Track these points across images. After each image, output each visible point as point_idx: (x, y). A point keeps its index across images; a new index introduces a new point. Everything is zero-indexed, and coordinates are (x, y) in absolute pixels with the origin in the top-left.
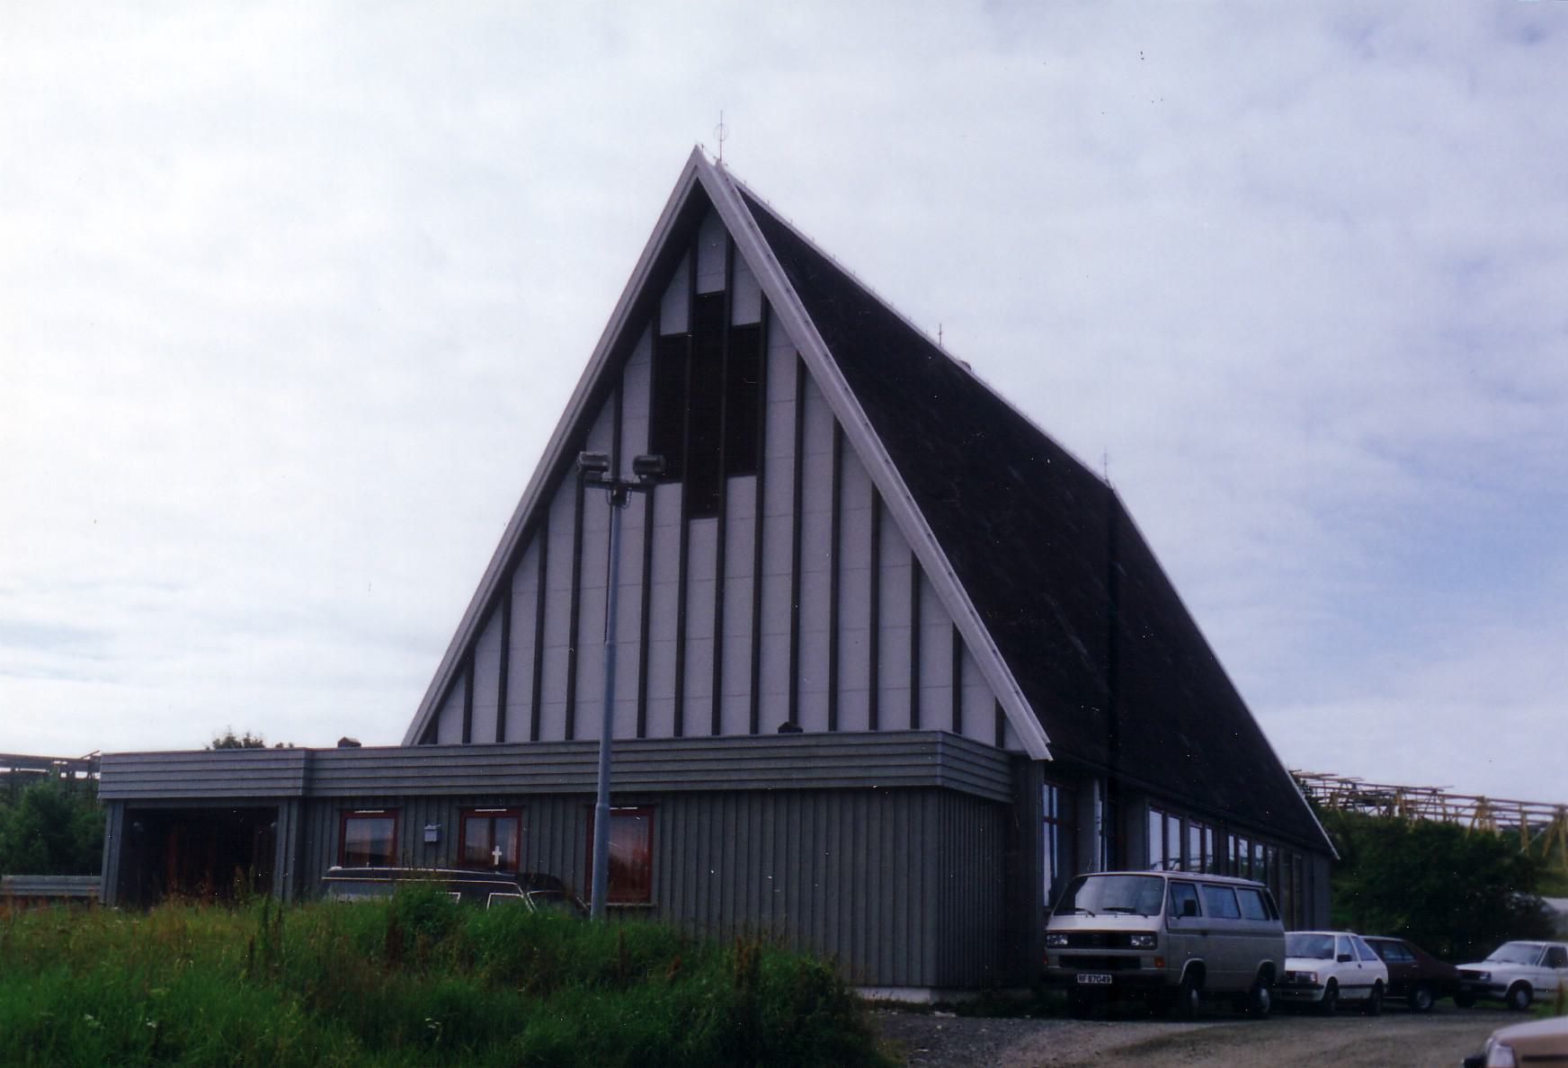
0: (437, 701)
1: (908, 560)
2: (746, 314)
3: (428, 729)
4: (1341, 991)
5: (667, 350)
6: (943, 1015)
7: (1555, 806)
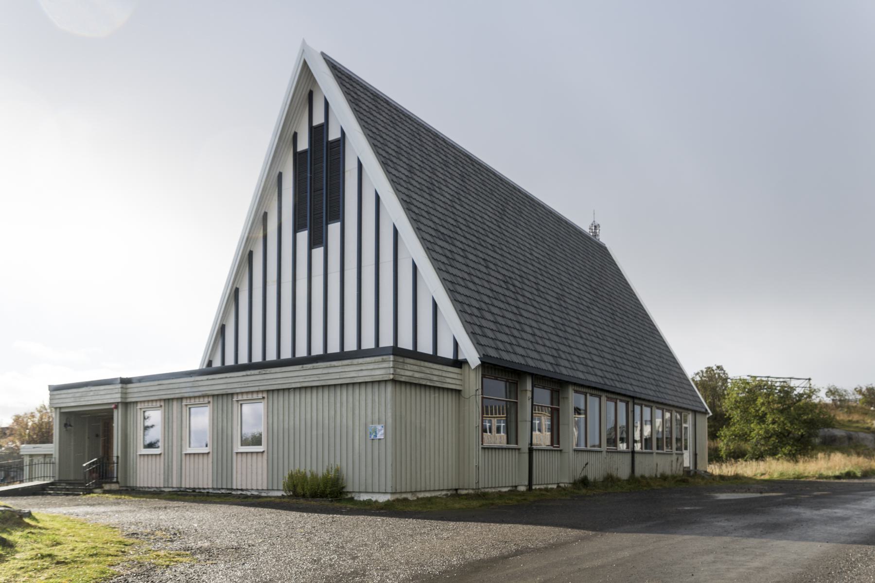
2: (334, 135)
5: (299, 157)
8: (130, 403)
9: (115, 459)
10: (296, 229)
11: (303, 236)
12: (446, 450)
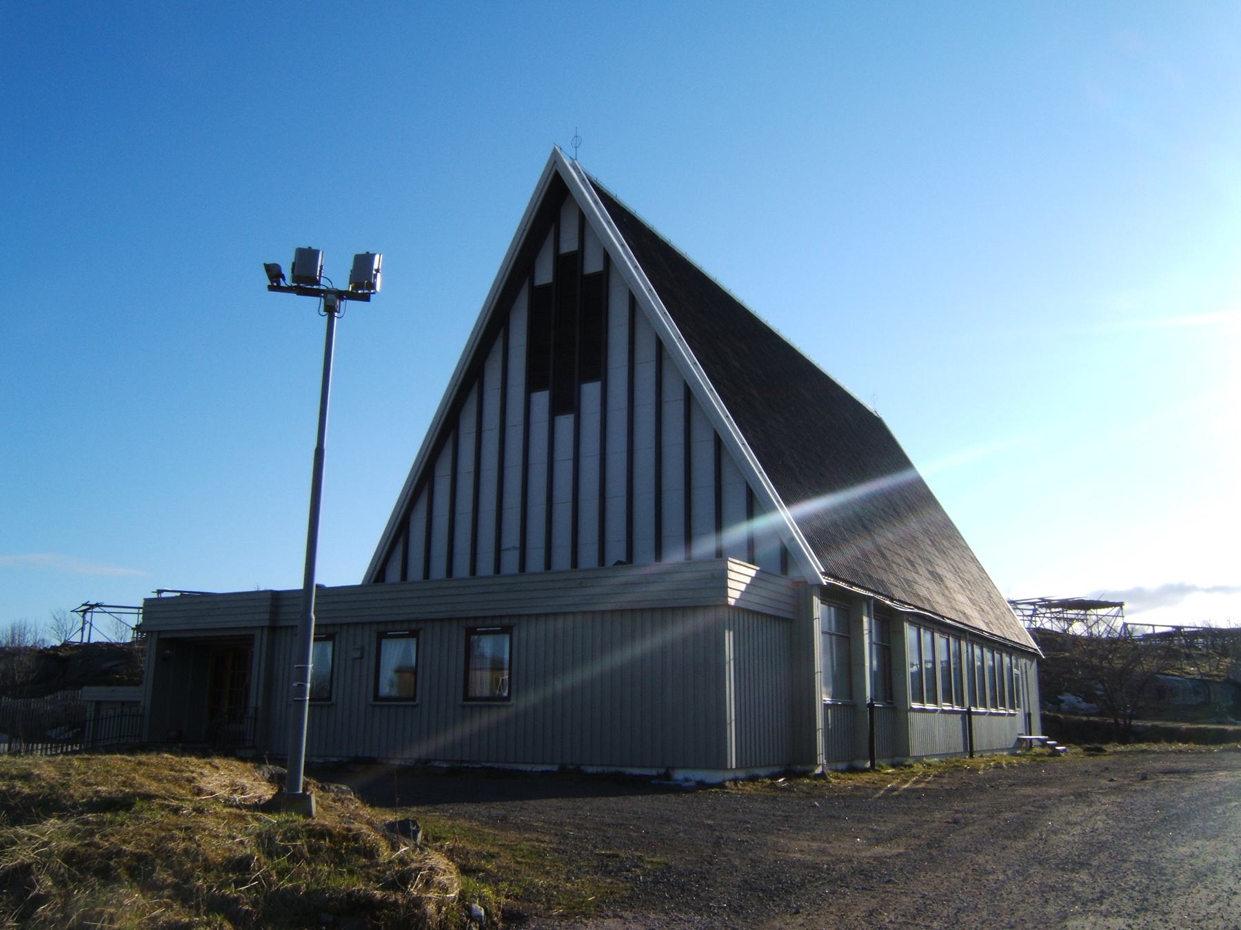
0: (383, 557)
1: (712, 436)
2: (593, 265)
3: (378, 572)
4: (328, 576)
5: (539, 296)
6: (621, 769)
7: (1173, 627)
8: (281, 627)
9: (251, 712)
10: (533, 385)
11: (542, 400)
12: (742, 638)
